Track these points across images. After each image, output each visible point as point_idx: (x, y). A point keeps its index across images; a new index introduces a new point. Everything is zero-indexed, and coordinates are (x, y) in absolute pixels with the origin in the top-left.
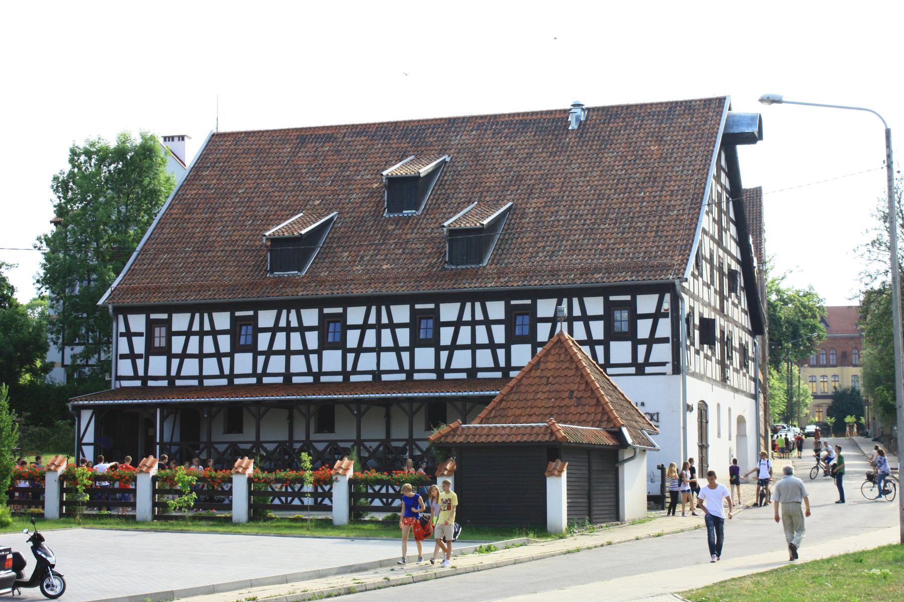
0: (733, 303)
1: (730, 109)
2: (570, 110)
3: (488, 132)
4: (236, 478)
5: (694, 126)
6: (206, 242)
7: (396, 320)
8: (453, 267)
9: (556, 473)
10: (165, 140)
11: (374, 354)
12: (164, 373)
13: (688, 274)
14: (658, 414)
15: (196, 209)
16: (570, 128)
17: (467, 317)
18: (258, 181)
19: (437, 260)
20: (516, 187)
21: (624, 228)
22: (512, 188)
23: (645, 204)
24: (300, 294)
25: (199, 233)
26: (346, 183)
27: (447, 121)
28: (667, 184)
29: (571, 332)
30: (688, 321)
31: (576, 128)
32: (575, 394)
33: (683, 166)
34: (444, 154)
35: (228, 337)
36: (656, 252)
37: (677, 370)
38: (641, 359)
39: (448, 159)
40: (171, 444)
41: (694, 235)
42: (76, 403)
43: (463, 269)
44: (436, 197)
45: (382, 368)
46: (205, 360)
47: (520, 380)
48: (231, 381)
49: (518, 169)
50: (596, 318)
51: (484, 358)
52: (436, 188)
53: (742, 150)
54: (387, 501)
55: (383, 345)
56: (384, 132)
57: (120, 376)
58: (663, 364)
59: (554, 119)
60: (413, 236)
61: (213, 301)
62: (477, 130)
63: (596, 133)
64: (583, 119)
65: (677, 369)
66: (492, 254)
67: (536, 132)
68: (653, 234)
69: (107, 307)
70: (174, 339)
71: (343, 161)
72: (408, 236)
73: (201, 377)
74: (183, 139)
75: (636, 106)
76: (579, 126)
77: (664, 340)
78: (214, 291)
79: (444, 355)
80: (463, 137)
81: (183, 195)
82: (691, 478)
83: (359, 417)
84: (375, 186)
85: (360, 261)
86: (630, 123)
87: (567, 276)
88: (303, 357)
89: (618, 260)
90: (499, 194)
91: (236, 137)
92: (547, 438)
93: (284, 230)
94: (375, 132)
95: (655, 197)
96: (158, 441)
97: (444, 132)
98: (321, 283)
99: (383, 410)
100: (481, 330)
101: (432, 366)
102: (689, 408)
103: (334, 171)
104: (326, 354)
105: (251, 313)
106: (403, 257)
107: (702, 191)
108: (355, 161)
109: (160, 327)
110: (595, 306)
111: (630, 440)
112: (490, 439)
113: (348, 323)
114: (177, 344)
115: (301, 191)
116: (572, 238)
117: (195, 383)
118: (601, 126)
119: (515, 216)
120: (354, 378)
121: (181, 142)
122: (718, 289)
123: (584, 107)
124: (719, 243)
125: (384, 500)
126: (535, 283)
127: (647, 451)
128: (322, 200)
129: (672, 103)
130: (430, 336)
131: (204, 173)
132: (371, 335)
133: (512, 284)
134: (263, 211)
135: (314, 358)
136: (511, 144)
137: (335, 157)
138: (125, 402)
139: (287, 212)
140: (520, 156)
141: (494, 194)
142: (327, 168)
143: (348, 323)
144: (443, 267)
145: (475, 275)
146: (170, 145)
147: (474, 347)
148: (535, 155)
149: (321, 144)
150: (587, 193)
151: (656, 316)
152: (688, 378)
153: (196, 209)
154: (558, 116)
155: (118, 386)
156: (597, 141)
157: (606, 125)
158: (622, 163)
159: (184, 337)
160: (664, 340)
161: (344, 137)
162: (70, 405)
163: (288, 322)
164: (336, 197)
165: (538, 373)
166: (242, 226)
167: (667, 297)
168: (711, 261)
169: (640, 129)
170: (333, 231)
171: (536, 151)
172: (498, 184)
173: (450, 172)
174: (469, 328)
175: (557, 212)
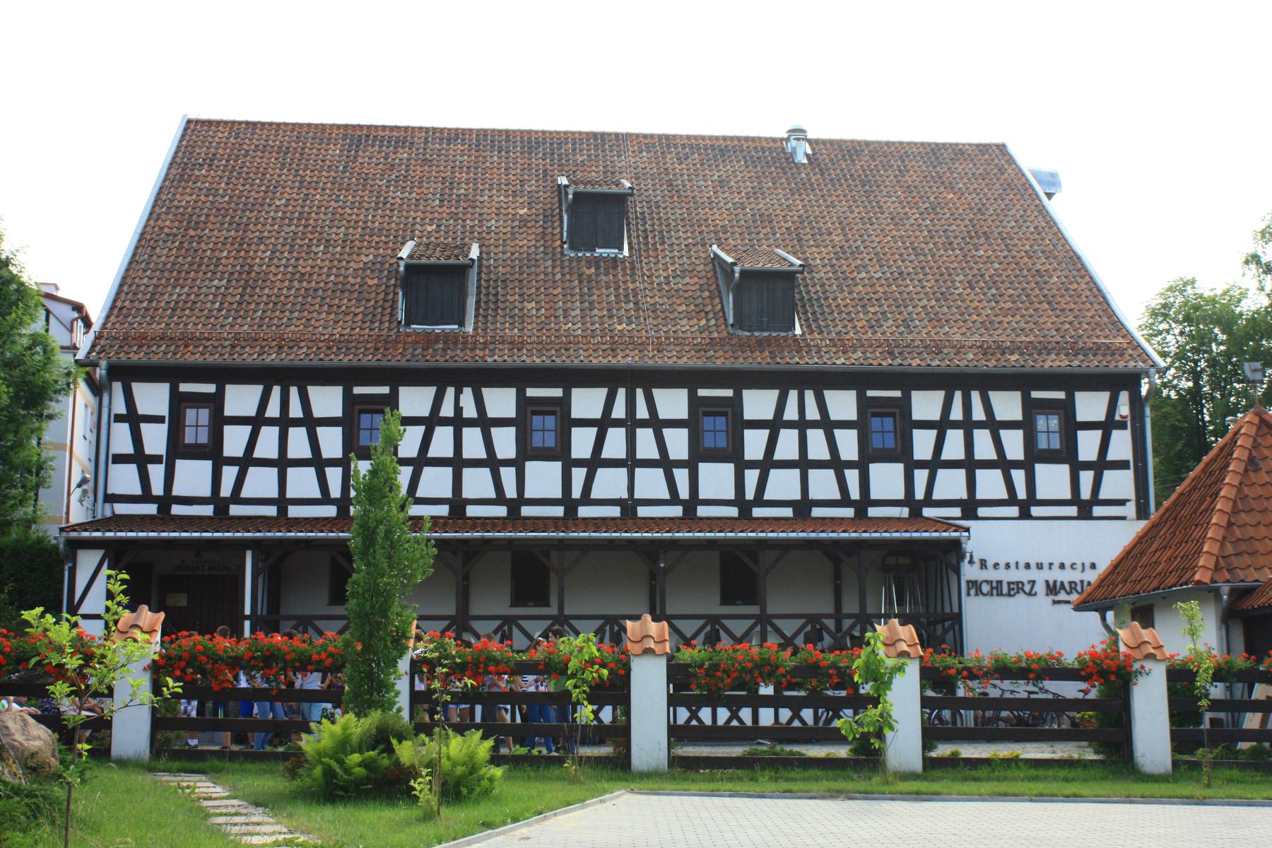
2: (788, 140)
7: (492, 413)
17: (791, 413)
38: (1086, 494)
45: (637, 495)
46: (638, 471)
57: (113, 495)
58: (1122, 502)
73: (282, 502)
77: (1122, 465)
82: (729, 676)
96: (247, 611)
109: (198, 408)
110: (501, 402)
114: (234, 441)
130: (203, 438)
135: (508, 475)
147: (804, 464)
151: (1107, 426)
160: (1122, 465)
163: (458, 409)
174: (795, 433)
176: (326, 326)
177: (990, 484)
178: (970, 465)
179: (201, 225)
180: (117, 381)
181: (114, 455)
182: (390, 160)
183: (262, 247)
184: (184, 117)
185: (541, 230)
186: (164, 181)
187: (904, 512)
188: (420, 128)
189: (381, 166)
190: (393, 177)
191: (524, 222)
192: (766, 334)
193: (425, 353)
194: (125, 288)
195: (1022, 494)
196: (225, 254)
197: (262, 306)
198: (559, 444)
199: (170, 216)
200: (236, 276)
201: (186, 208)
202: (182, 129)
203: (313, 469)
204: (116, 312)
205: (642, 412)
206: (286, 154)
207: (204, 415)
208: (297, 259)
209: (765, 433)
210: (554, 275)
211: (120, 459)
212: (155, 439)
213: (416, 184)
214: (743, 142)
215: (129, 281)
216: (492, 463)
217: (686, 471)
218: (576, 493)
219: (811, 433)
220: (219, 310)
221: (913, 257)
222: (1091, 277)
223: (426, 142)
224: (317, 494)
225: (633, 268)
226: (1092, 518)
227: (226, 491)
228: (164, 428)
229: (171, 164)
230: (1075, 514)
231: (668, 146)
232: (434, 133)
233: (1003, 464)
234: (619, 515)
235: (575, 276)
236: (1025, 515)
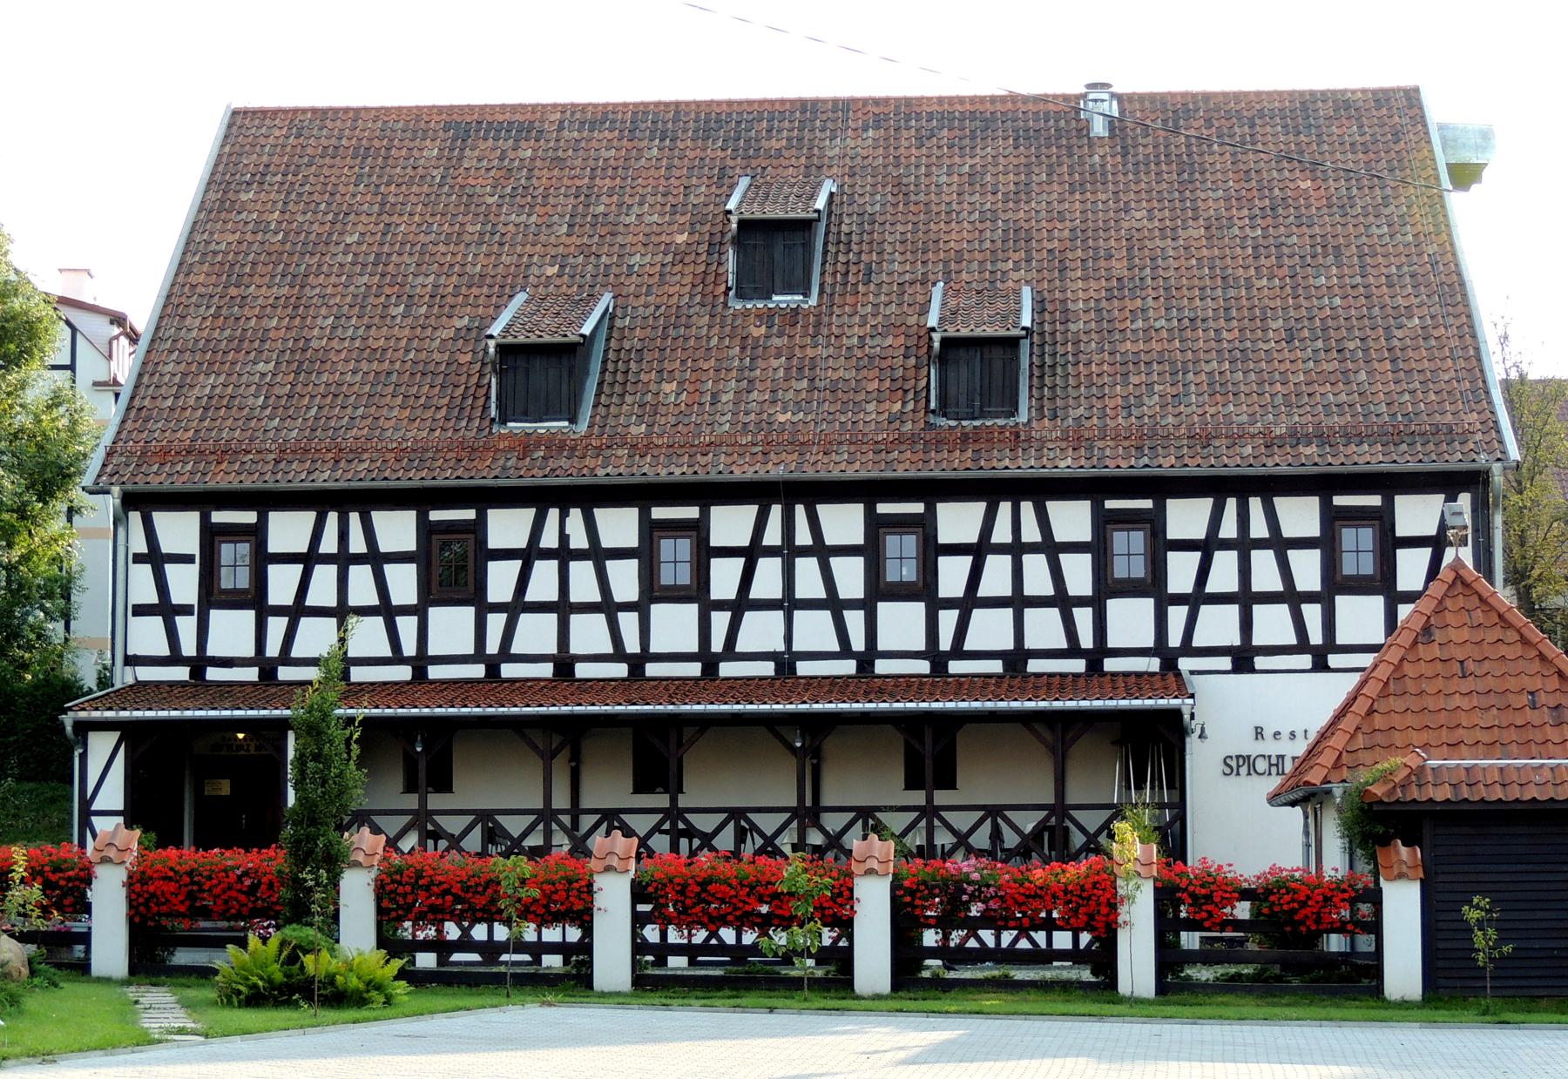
2: (1084, 96)
3: (905, 134)
11: (779, 616)
12: (249, 651)
35: (411, 569)
42: (83, 715)
45: (796, 647)
46: (798, 614)
48: (420, 673)
50: (621, 554)
70: (716, 563)
81: (207, 243)
104: (1116, 608)
105: (470, 514)
110: (619, 526)
113: (1170, 536)
114: (282, 584)
120: (727, 669)
126: (1166, 464)
131: (243, 197)
132: (325, 576)
143: (1170, 536)
147: (1018, 602)
159: (301, 567)
161: (560, 129)
162: (68, 720)
163: (564, 538)
174: (1007, 560)
177: (1273, 624)
178: (1246, 599)
179: (246, 279)
180: (136, 510)
181: (134, 606)
182: (506, 162)
183: (324, 311)
184: (228, 107)
185: (702, 268)
186: (199, 211)
187: (1153, 664)
188: (555, 106)
189: (492, 173)
190: (508, 190)
191: (680, 256)
192: (977, 423)
193: (520, 466)
194: (145, 379)
195: (1316, 637)
196: (274, 322)
197: (317, 400)
198: (695, 583)
199: (205, 268)
200: (287, 356)
201: (226, 253)
202: (224, 126)
204: (133, 413)
205: (803, 537)
206: (365, 158)
207: (244, 548)
208: (369, 327)
210: (709, 339)
211: (140, 610)
212: (184, 584)
213: (539, 200)
214: (1020, 104)
215: (150, 368)
216: (608, 607)
217: (862, 613)
218: (717, 645)
219: (355, 571)
220: (264, 408)
221: (1219, 292)
222: (1469, 316)
223: (560, 129)
224: (387, 652)
225: (818, 324)
226: (1252, 670)
227: (273, 650)
229: (209, 184)
230: (1309, 666)
231: (908, 119)
232: (573, 113)
233: (1291, 597)
235: (737, 341)
236: (1320, 666)
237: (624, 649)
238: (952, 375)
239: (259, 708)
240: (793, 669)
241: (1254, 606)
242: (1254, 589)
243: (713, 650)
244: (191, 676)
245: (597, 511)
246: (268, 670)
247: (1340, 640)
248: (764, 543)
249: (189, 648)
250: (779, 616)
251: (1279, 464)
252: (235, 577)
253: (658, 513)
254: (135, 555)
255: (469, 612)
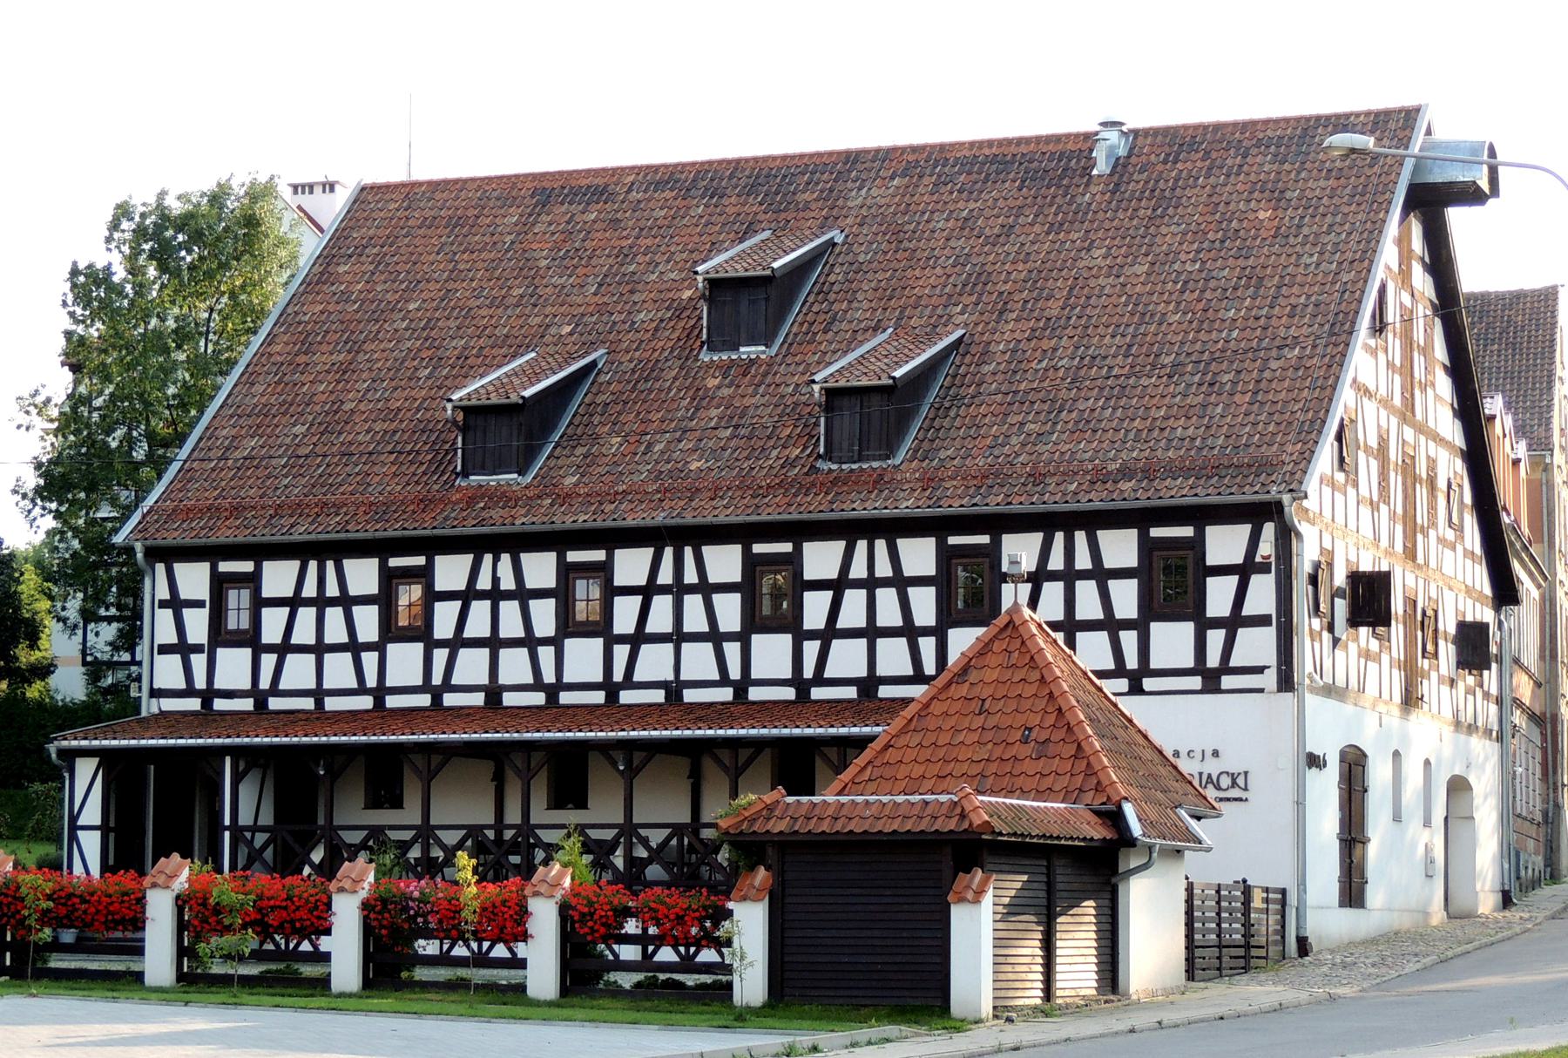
0: (1441, 541)
1: (1429, 132)
2: (1097, 133)
3: (926, 180)
4: (534, 905)
5: (1350, 168)
6: (336, 412)
8: (834, 467)
9: (970, 895)
10: (295, 192)
13: (1312, 485)
14: (1246, 773)
15: (320, 343)
16: (1095, 172)
17: (858, 570)
18: (451, 285)
19: (802, 451)
20: (974, 298)
21: (1189, 385)
22: (966, 299)
23: (1235, 334)
24: (518, 522)
25: (323, 393)
26: (629, 287)
27: (1201, 131)
28: (1284, 290)
29: (1033, 603)
30: (1313, 580)
31: (1108, 172)
32: (1034, 735)
33: (1321, 253)
34: (831, 228)
35: (551, 602)
36: (1251, 436)
37: (1286, 682)
38: (1213, 660)
39: (839, 239)
40: (255, 829)
41: (1331, 400)
42: (65, 743)
43: (852, 471)
44: (810, 317)
45: (683, 677)
47: (927, 705)
49: (981, 259)
51: (893, 657)
52: (811, 299)
53: (1457, 217)
54: (687, 951)
55: (687, 628)
56: (712, 180)
57: (160, 690)
58: (1259, 670)
59: (1062, 154)
60: (757, 400)
61: (342, 536)
62: (903, 175)
63: (1147, 182)
64: (1122, 152)
65: (1286, 682)
66: (916, 438)
67: (1023, 181)
68: (1247, 398)
69: (133, 549)
70: (266, 612)
71: (625, 243)
72: (747, 401)
73: (319, 694)
74: (332, 189)
75: (1235, 124)
76: (1114, 167)
77: (1262, 621)
78: (346, 514)
79: (811, 649)
80: (874, 192)
83: (630, 775)
84: (687, 294)
85: (644, 454)
86: (1218, 162)
87: (1062, 487)
88: (525, 651)
89: (1170, 454)
90: (939, 311)
91: (409, 192)
92: (952, 825)
93: (491, 388)
94: (693, 181)
95: (1257, 318)
96: (227, 822)
97: (835, 180)
98: (566, 498)
99: (684, 764)
100: (510, 609)
101: (787, 674)
102: (1314, 761)
103: (604, 263)
106: (733, 443)
107: (1353, 306)
108: (649, 242)
111: (1136, 829)
112: (838, 827)
115: (535, 306)
116: (1081, 405)
117: (308, 704)
118: (1160, 167)
119: (968, 359)
120: (627, 697)
121: (328, 195)
122: (1399, 510)
123: (1124, 129)
124: (1407, 414)
125: (682, 949)
127: (1187, 853)
128: (577, 325)
129: (1308, 119)
130: (245, 624)
133: (950, 502)
134: (455, 348)
135: (732, 650)
136: (972, 205)
137: (607, 235)
138: (162, 742)
139: (504, 351)
140: (987, 231)
141: (927, 312)
142: (590, 258)
144: (812, 467)
145: (879, 482)
146: (305, 200)
147: (872, 633)
148: (1017, 229)
149: (581, 207)
150: (1119, 310)
151: (1245, 571)
152: (1311, 700)
153: (320, 343)
154: (1070, 146)
155: (156, 711)
156: (1149, 200)
157: (1169, 166)
158: (1195, 246)
159: (830, 593)
160: (1262, 621)
161: (630, 191)
162: (52, 749)
163: (496, 580)
164: (605, 318)
165: (963, 690)
166: (410, 379)
167: (1269, 529)
168: (1382, 452)
169: (1238, 174)
170: (594, 390)
171: (1021, 220)
172: (938, 291)
173: (842, 264)
174: (487, 604)
175: (1055, 350)
176: (386, 481)
181: (159, 645)
184: (359, 183)
195: (1132, 662)
203: (349, 654)
207: (246, 594)
209: (828, 595)
219: (881, 593)
226: (1218, 690)
227: (265, 683)
228: (204, 613)
234: (252, 708)
237: (542, 679)
238: (837, 423)
239: (196, 738)
240: (680, 697)
241: (1078, 634)
242: (1078, 617)
243: (615, 680)
244: (203, 706)
245: (523, 556)
246: (260, 698)
247: (1154, 664)
248: (658, 582)
249: (200, 683)
250: (863, 642)
251: (1096, 501)
252: (237, 620)
253: (573, 556)
254: (160, 601)
255: (1188, 628)
